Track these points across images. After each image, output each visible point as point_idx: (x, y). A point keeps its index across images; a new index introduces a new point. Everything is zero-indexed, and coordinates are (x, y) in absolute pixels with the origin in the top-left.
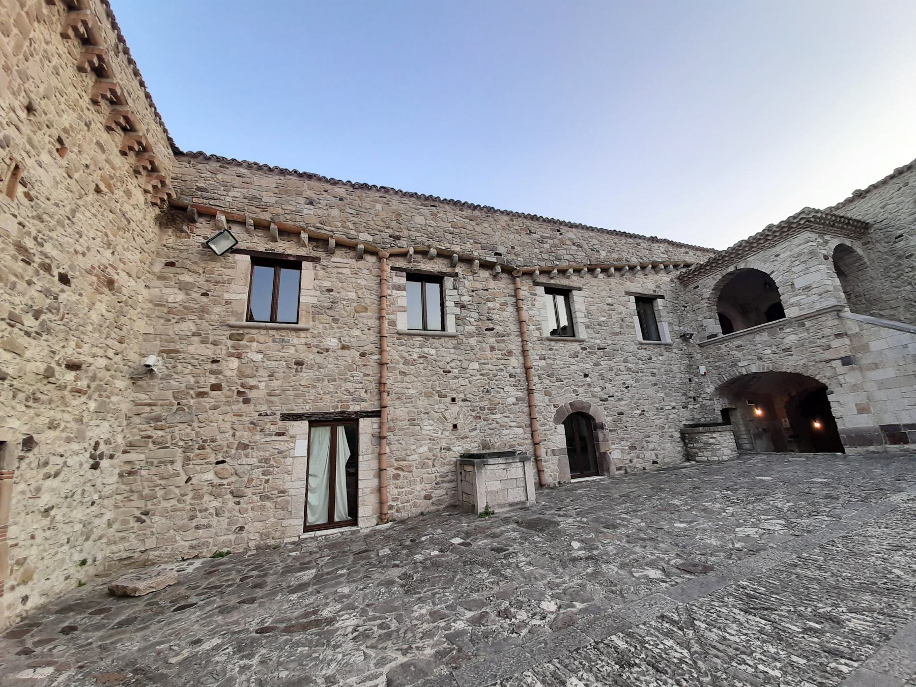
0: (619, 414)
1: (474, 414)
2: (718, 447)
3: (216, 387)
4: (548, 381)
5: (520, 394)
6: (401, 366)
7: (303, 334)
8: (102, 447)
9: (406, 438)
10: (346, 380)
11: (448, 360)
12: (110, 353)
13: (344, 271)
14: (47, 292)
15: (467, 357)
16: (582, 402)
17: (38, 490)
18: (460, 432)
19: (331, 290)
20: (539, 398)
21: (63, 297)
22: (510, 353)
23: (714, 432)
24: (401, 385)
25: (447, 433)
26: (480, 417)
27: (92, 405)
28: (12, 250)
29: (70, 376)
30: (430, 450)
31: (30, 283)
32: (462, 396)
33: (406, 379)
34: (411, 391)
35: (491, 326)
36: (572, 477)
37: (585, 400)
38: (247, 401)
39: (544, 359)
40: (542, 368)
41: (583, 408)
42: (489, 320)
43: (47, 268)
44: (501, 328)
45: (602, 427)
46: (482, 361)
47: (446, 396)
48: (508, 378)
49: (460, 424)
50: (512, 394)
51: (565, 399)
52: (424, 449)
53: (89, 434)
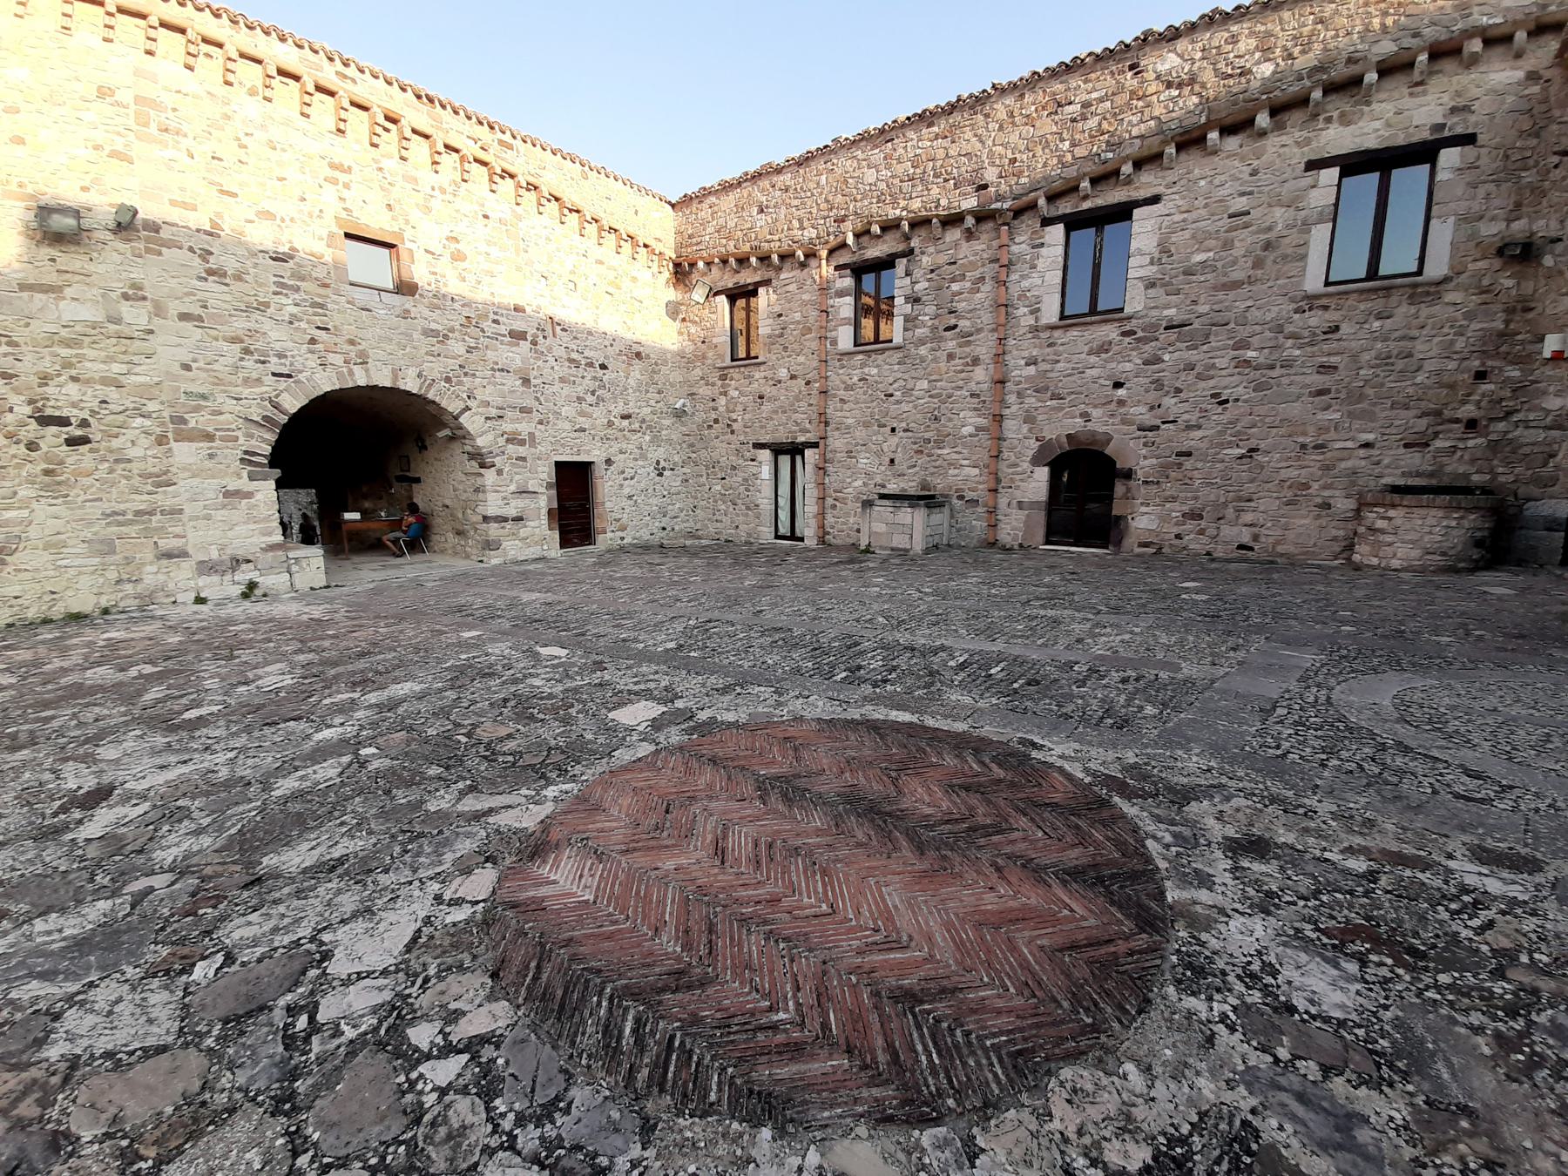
0: (1179, 454)
1: (915, 447)
2: (1389, 538)
3: (716, 421)
4: (1033, 400)
5: (982, 421)
6: (842, 392)
7: (762, 368)
8: (662, 464)
9: (843, 470)
10: (795, 411)
11: (891, 380)
12: (652, 402)
13: (790, 288)
14: (594, 378)
15: (914, 374)
16: (1094, 433)
17: (621, 485)
18: (898, 467)
19: (780, 315)
20: (1014, 428)
21: (605, 378)
22: (976, 361)
23: (1393, 506)
24: (839, 414)
25: (883, 468)
26: (922, 452)
27: (647, 438)
28: (567, 364)
29: (625, 423)
30: (865, 484)
31: (583, 377)
32: (904, 425)
33: (845, 407)
34: (850, 421)
35: (953, 322)
36: (1048, 543)
37: (1101, 429)
38: (733, 432)
39: (1035, 364)
40: (1028, 378)
41: (1094, 442)
42: (950, 313)
43: (591, 365)
44: (967, 323)
45: (1128, 475)
46: (933, 378)
47: (885, 426)
48: (968, 399)
49: (898, 457)
50: (969, 422)
51: (1061, 426)
52: (859, 483)
53: (650, 456)
